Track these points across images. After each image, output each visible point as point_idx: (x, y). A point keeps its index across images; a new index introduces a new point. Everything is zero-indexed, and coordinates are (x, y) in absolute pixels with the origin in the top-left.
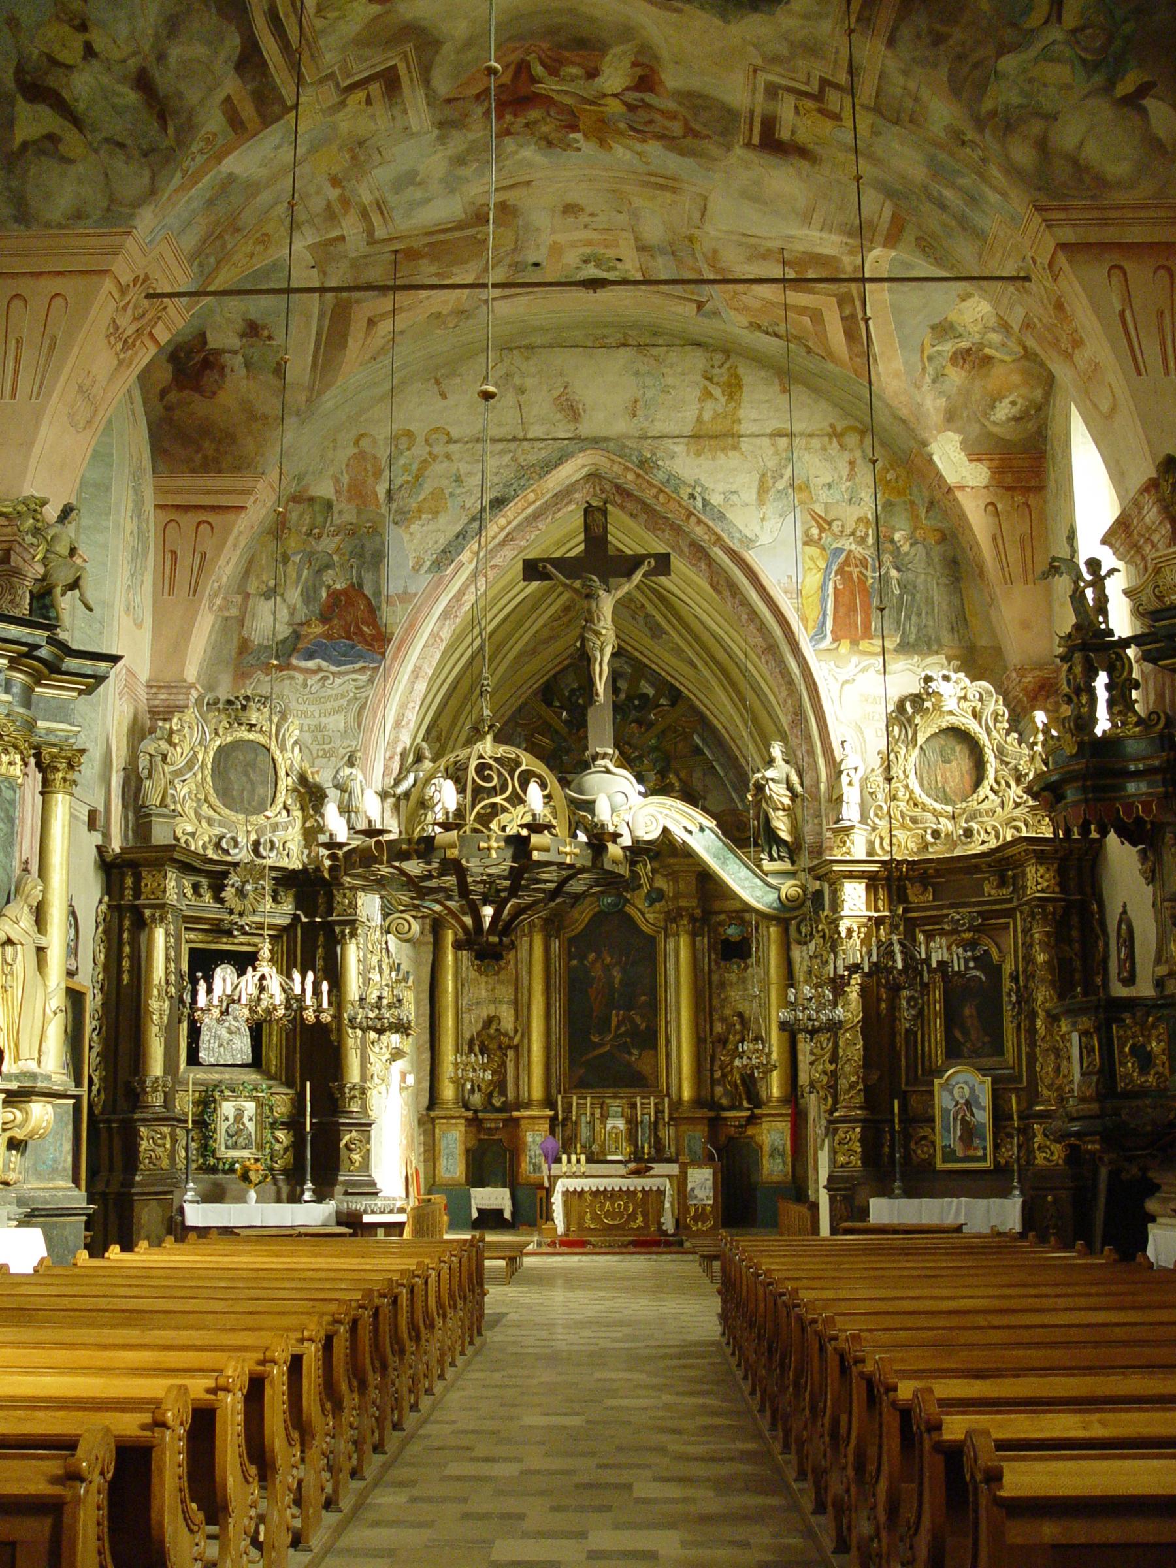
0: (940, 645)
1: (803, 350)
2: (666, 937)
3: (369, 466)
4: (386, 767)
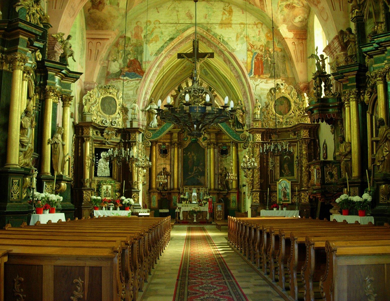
1: (248, 3)
2: (208, 149)
3: (140, 29)
4: (143, 104)
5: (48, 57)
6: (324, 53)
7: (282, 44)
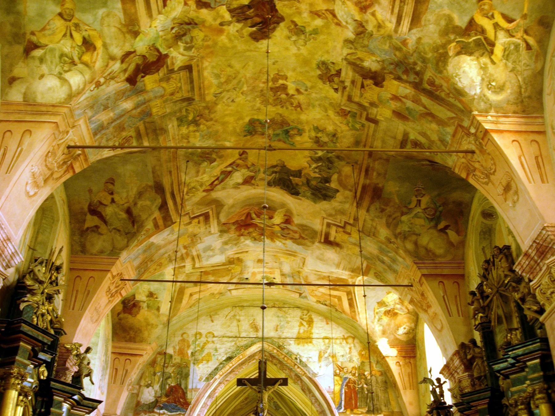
0: (382, 411)
1: (334, 310)
5: (57, 375)
6: (441, 375)
7: (382, 365)
